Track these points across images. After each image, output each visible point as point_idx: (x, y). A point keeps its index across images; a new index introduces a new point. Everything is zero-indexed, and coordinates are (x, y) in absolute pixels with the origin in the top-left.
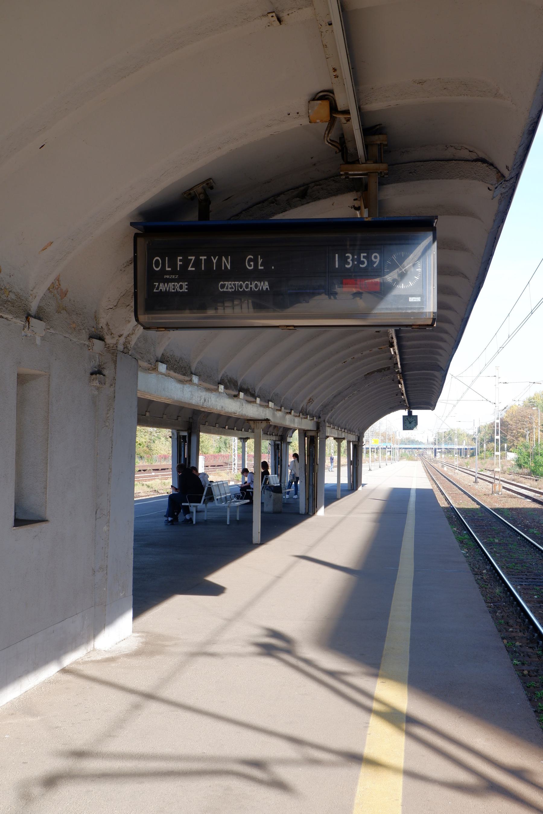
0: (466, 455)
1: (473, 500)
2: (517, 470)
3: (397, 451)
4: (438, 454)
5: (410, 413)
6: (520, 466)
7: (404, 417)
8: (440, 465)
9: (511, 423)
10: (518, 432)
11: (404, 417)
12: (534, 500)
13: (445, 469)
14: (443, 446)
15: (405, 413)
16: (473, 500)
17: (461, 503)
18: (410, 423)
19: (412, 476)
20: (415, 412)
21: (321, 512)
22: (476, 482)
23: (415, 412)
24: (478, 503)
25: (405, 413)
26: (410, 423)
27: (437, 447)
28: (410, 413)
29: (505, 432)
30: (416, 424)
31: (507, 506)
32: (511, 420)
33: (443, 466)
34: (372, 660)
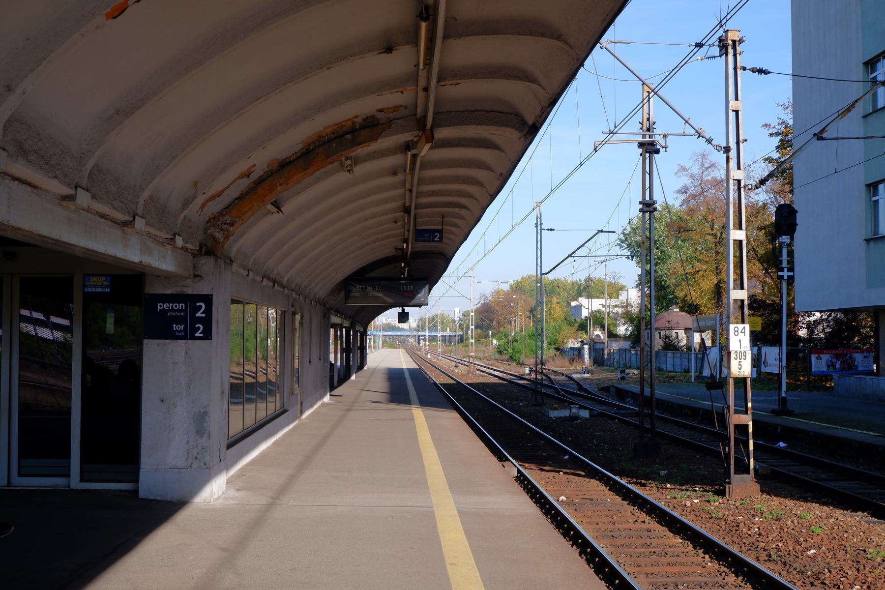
0: (450, 342)
1: (452, 378)
2: (498, 356)
3: (634, 363)
4: (421, 342)
5: (403, 310)
6: (500, 353)
7: (399, 313)
8: (424, 352)
9: (497, 308)
10: (505, 319)
11: (399, 313)
12: (500, 378)
13: (429, 356)
14: (427, 333)
15: (399, 310)
16: (452, 378)
17: (441, 380)
18: (403, 317)
19: (401, 360)
20: (407, 309)
21: (353, 377)
22: (456, 366)
23: (407, 309)
24: (455, 380)
25: (399, 310)
26: (403, 317)
27: (420, 334)
28: (403, 310)
29: (488, 317)
30: (408, 319)
31: (478, 381)
32: (498, 305)
33: (427, 354)
34: (407, 401)
